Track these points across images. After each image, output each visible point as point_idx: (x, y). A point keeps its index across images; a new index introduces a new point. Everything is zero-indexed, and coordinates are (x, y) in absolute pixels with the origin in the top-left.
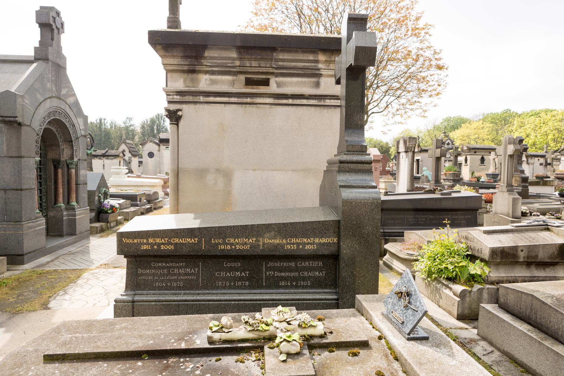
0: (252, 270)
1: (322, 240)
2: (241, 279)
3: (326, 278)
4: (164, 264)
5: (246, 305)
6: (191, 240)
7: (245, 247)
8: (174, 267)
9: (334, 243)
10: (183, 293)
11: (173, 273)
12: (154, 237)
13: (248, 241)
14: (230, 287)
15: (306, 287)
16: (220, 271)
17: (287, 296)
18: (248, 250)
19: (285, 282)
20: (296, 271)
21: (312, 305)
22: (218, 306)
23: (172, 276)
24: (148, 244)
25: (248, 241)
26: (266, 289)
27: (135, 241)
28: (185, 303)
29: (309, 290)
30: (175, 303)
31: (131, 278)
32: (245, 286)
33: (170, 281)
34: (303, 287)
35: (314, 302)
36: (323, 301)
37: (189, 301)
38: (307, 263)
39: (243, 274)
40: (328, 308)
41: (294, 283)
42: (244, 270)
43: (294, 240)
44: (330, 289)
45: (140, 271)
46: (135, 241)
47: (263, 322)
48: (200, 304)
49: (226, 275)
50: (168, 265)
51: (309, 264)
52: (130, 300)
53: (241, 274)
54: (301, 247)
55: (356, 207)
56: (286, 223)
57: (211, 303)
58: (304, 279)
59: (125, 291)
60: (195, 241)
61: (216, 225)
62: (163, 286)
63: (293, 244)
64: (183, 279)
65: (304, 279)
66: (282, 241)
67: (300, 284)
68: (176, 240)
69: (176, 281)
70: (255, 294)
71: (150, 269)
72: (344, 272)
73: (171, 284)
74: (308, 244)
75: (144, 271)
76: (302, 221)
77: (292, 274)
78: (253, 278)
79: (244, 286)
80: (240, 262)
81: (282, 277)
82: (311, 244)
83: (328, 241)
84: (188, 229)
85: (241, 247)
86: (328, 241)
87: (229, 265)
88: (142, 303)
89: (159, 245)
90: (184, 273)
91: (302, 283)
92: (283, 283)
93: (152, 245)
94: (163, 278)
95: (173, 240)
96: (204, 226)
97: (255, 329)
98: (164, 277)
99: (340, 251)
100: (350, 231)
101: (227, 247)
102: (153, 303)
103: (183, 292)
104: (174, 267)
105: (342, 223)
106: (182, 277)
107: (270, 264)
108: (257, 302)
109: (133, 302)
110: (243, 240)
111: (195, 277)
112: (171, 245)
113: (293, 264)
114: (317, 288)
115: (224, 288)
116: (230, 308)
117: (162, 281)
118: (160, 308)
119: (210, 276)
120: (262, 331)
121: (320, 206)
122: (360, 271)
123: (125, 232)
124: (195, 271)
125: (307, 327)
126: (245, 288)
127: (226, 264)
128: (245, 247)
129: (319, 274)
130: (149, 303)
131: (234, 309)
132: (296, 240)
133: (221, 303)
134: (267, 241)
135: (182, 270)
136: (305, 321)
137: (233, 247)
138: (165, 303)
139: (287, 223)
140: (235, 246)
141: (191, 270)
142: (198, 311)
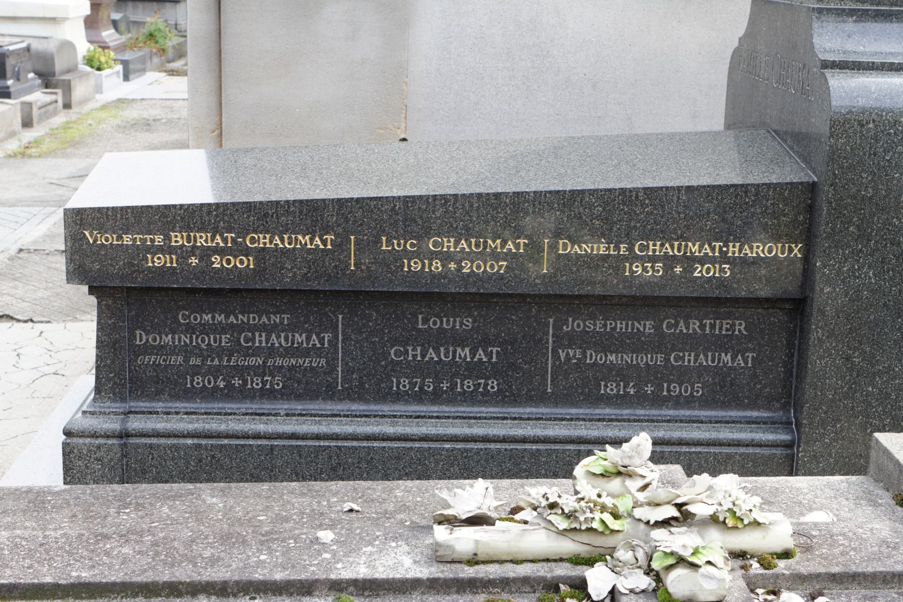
0: (512, 344)
1: (751, 248)
2: (473, 370)
3: (755, 375)
4: (220, 318)
5: (490, 456)
6: (312, 240)
7: (492, 267)
8: (253, 329)
9: (791, 261)
10: (283, 413)
11: (248, 348)
12: (189, 229)
13: (503, 247)
14: (437, 397)
15: (689, 402)
16: (405, 344)
17: (624, 428)
18: (502, 277)
19: (618, 385)
20: (657, 349)
21: (706, 461)
22: (512, 456)
23: (247, 355)
24: (167, 249)
25: (503, 247)
26: (556, 405)
27: (127, 240)
28: (294, 443)
29: (696, 413)
30: (259, 442)
31: (113, 362)
32: (486, 393)
33: (241, 371)
34: (678, 402)
35: (712, 450)
36: (742, 450)
37: (304, 437)
38: (695, 325)
39: (481, 354)
40: (759, 470)
41: (649, 389)
42: (485, 343)
43: (655, 248)
44: (769, 409)
45: (141, 338)
46: (127, 240)
47: (604, 508)
48: (339, 448)
49: (423, 356)
50: (232, 319)
51: (702, 327)
52: (113, 432)
53: (473, 353)
54: (678, 270)
55: (877, 141)
56: (630, 191)
57: (376, 444)
58: (683, 375)
59: (94, 400)
60: (324, 242)
61: (396, 193)
62: (216, 388)
63: (653, 259)
64: (282, 367)
65: (683, 375)
66: (617, 248)
67: (669, 391)
68: (264, 241)
69: (261, 371)
70: (521, 419)
71: (174, 333)
72: (821, 358)
73: (245, 382)
74: (702, 261)
75: (155, 340)
76: (684, 182)
77: (644, 359)
78: (514, 367)
79: (483, 394)
80: (470, 316)
81: (611, 367)
82: (713, 260)
83: (770, 251)
84: (301, 202)
85: (479, 267)
86: (770, 251)
87: (435, 323)
88: (154, 441)
89: (206, 254)
90: (286, 349)
91: (676, 389)
92: (611, 389)
93: (183, 253)
94: (216, 362)
95: (253, 240)
96: (356, 195)
97: (583, 527)
98: (220, 360)
99: (812, 289)
100: (850, 222)
101: (431, 265)
102: (189, 441)
103: (283, 406)
104: (253, 329)
105: (826, 193)
106: (279, 362)
107: (573, 325)
108: (528, 446)
109: (124, 435)
110: (485, 242)
111: (323, 361)
112: (246, 256)
113: (648, 326)
114: (724, 406)
115: (420, 397)
116: (437, 463)
117: (216, 372)
118: (213, 457)
119: (370, 359)
120: (602, 533)
121: (728, 127)
122: (874, 357)
123: (93, 209)
124: (322, 341)
125: (740, 526)
126: (486, 398)
127: (426, 321)
128: (492, 267)
129: (733, 359)
130: (175, 441)
131: (452, 465)
132: (662, 245)
133: (408, 445)
134: (565, 249)
135: (278, 337)
136: (735, 509)
137: (452, 266)
138: (226, 441)
139: (637, 190)
140: (459, 263)
141: (308, 339)
142: (334, 469)
